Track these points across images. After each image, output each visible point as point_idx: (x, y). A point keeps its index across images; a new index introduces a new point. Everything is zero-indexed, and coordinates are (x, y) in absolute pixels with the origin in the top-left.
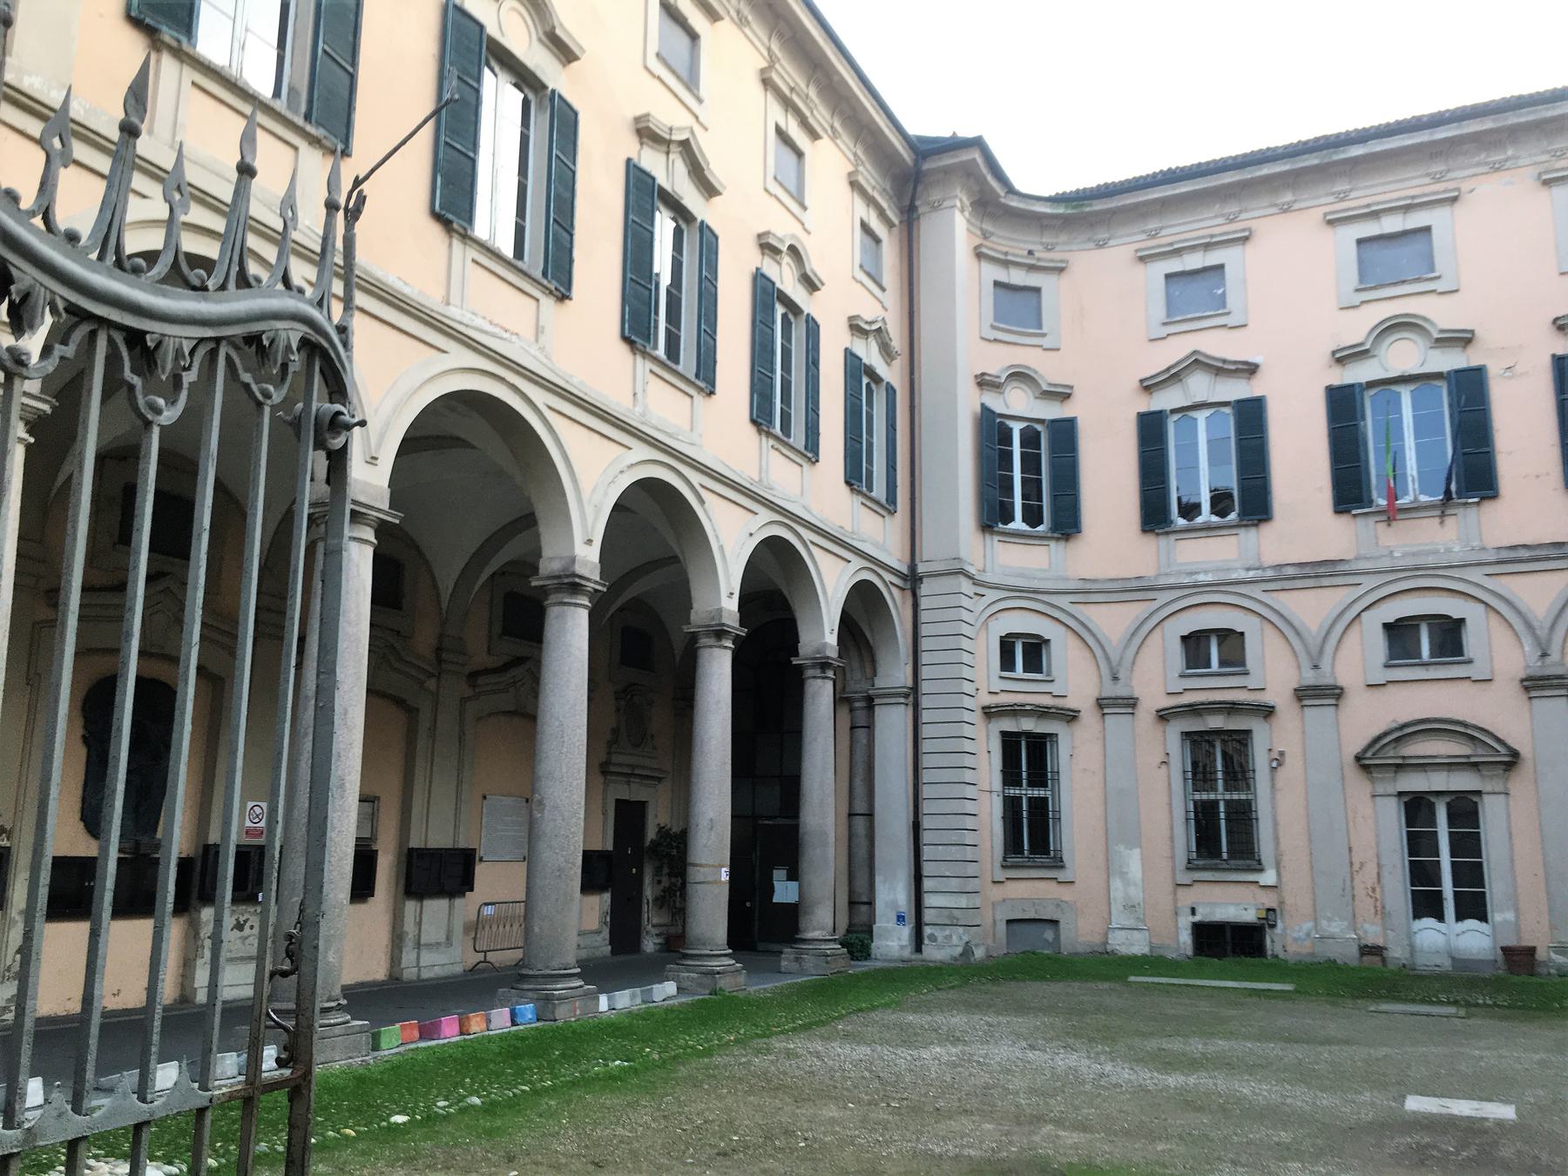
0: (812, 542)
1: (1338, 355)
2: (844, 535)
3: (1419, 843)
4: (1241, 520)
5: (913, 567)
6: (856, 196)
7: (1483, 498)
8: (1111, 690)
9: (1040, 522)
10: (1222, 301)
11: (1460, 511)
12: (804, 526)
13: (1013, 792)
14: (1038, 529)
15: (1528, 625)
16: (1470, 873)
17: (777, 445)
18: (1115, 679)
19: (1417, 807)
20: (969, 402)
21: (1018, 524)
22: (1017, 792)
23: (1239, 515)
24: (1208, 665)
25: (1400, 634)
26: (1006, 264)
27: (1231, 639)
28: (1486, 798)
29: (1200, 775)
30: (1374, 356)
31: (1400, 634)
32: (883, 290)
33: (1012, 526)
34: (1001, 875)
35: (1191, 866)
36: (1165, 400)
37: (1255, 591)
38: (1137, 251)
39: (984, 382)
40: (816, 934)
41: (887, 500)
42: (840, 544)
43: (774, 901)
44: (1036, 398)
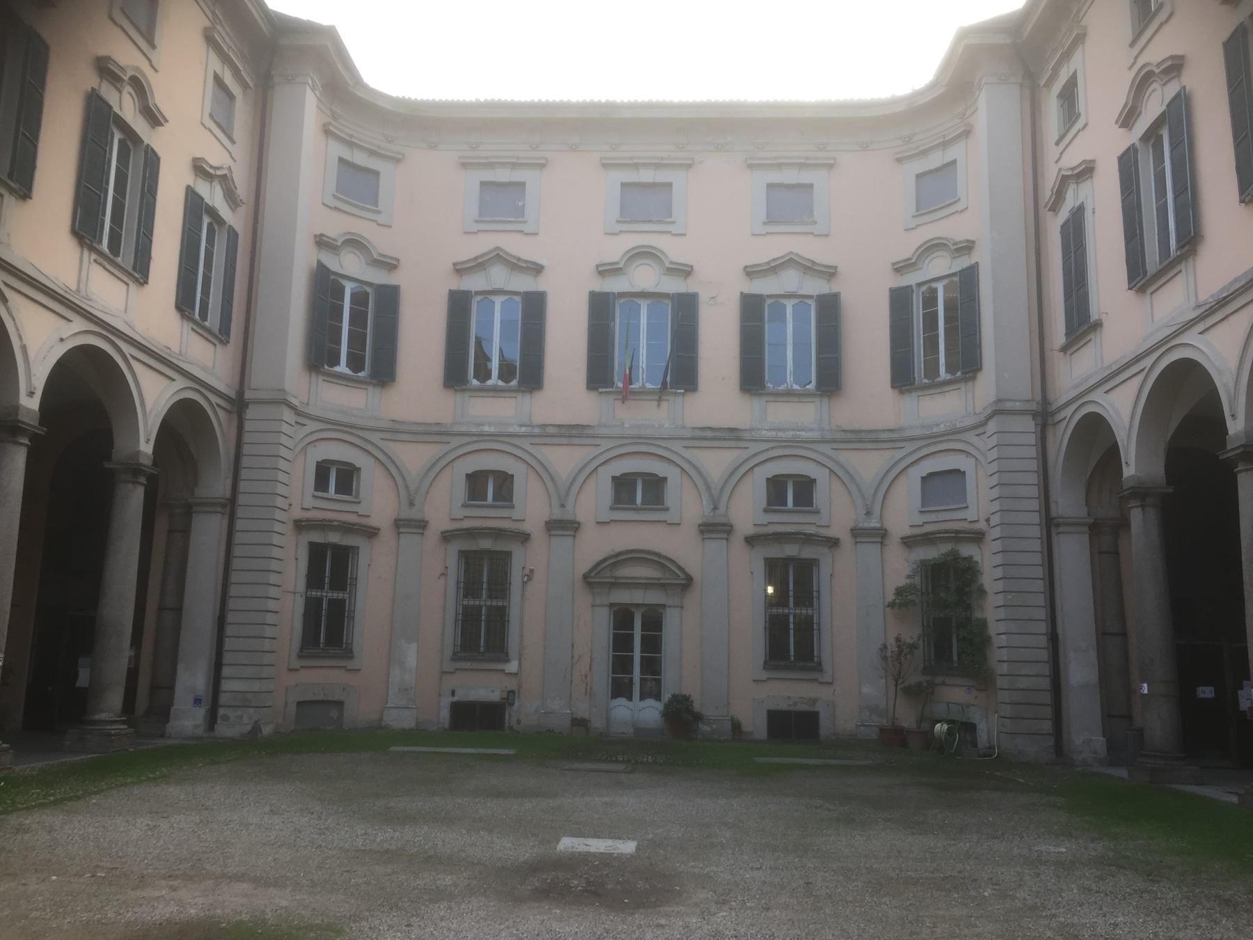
0: (131, 355)
1: (600, 269)
2: (170, 355)
3: (621, 642)
4: (519, 386)
5: (240, 393)
6: (211, 51)
7: (686, 391)
8: (407, 513)
9: (362, 368)
10: (521, 212)
11: (672, 398)
12: (125, 341)
13: (315, 593)
14: (359, 374)
15: (708, 487)
16: (652, 666)
17: (100, 260)
18: (411, 504)
19: (623, 617)
20: (304, 258)
21: (342, 368)
22: (319, 594)
23: (518, 382)
24: (485, 499)
25: (623, 486)
26: (350, 144)
27: (504, 482)
28: (668, 610)
29: (469, 587)
30: (625, 274)
31: (623, 486)
32: (233, 142)
33: (337, 369)
34: (296, 663)
35: (455, 658)
36: (473, 283)
37: (525, 444)
38: (459, 157)
39: (322, 242)
40: (103, 716)
41: (220, 330)
42: (162, 362)
43: (78, 685)
44: (368, 264)
